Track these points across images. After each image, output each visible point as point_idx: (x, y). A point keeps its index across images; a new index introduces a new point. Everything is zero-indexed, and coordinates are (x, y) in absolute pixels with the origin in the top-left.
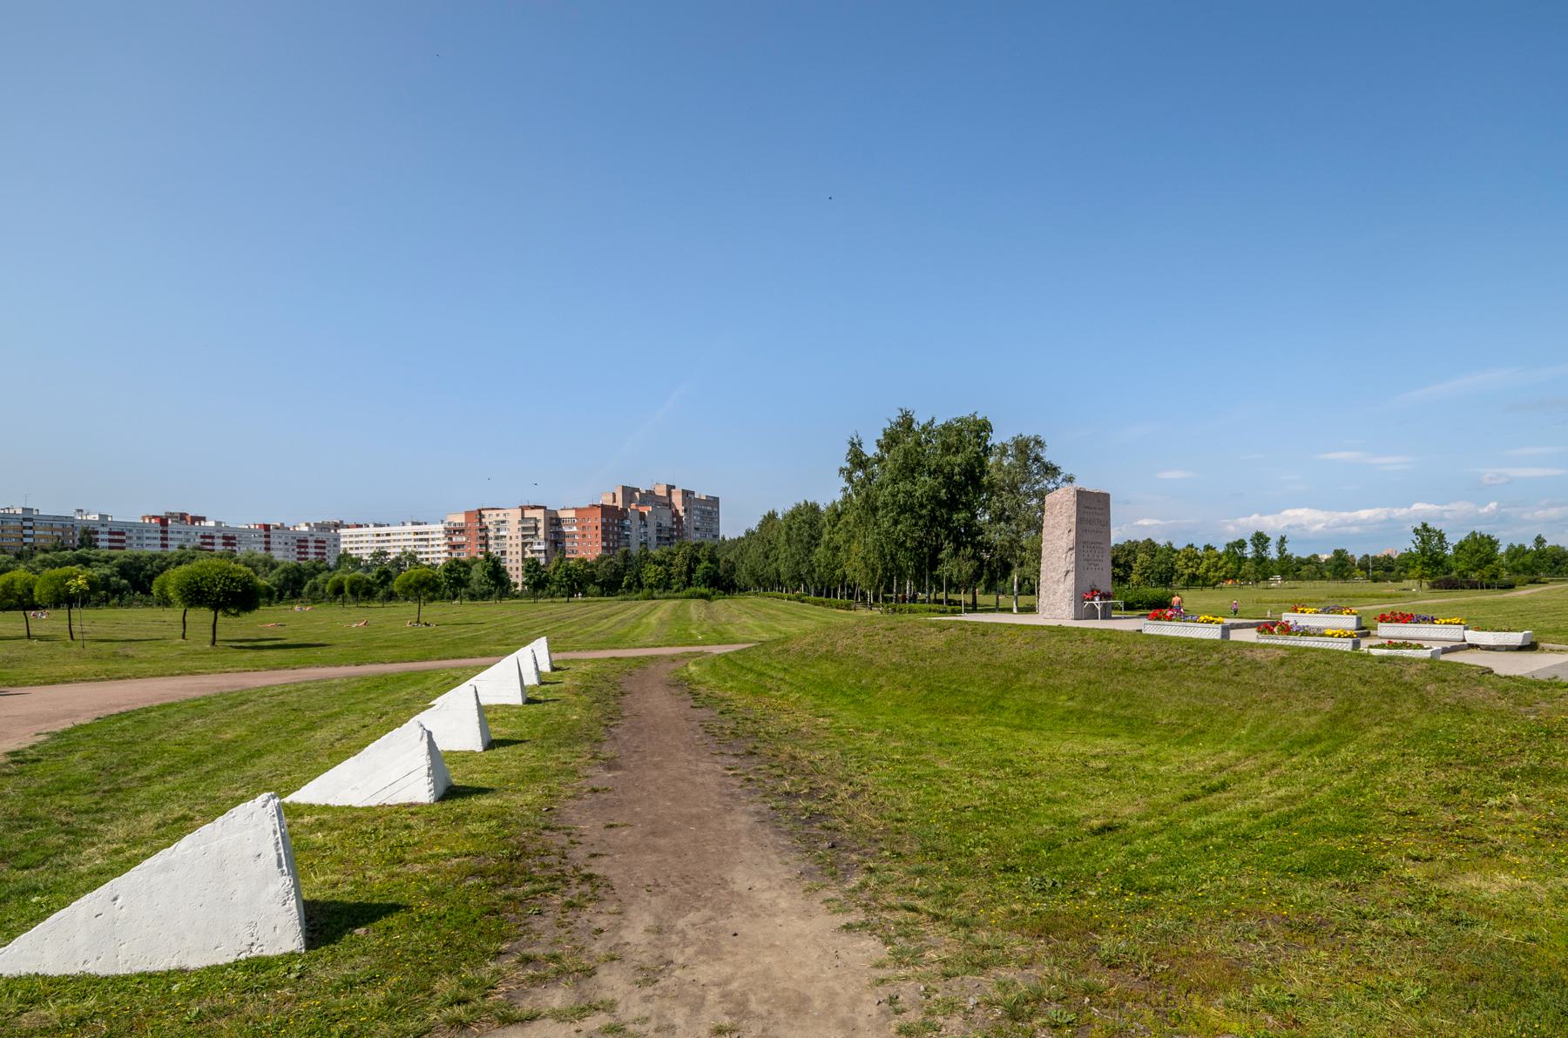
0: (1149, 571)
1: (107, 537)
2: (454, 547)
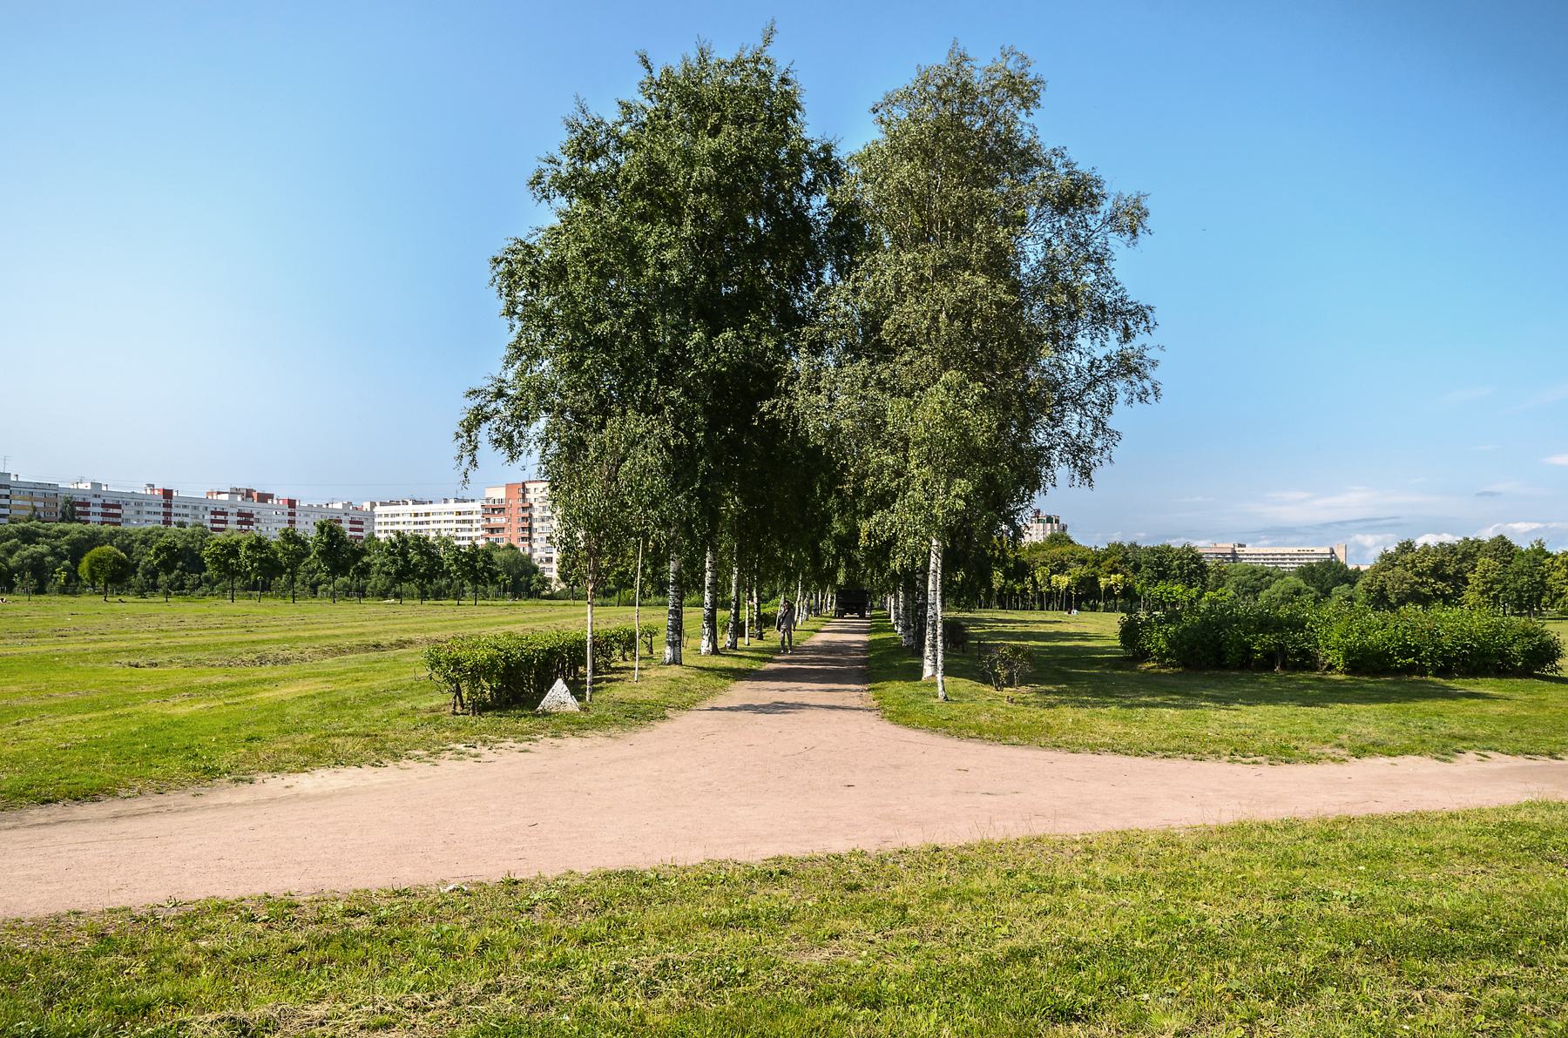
0: (1498, 587)
1: (100, 510)
2: (492, 531)
